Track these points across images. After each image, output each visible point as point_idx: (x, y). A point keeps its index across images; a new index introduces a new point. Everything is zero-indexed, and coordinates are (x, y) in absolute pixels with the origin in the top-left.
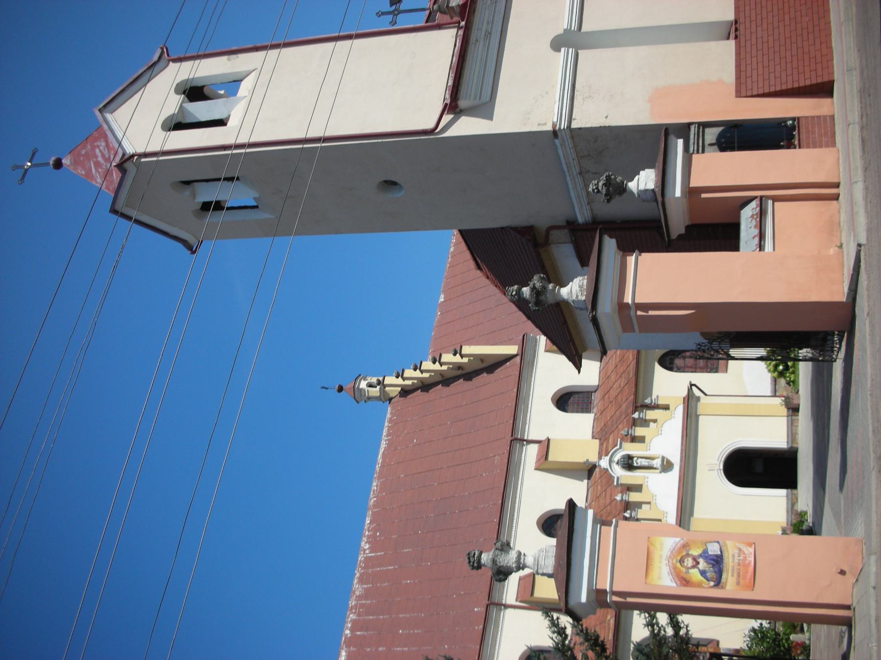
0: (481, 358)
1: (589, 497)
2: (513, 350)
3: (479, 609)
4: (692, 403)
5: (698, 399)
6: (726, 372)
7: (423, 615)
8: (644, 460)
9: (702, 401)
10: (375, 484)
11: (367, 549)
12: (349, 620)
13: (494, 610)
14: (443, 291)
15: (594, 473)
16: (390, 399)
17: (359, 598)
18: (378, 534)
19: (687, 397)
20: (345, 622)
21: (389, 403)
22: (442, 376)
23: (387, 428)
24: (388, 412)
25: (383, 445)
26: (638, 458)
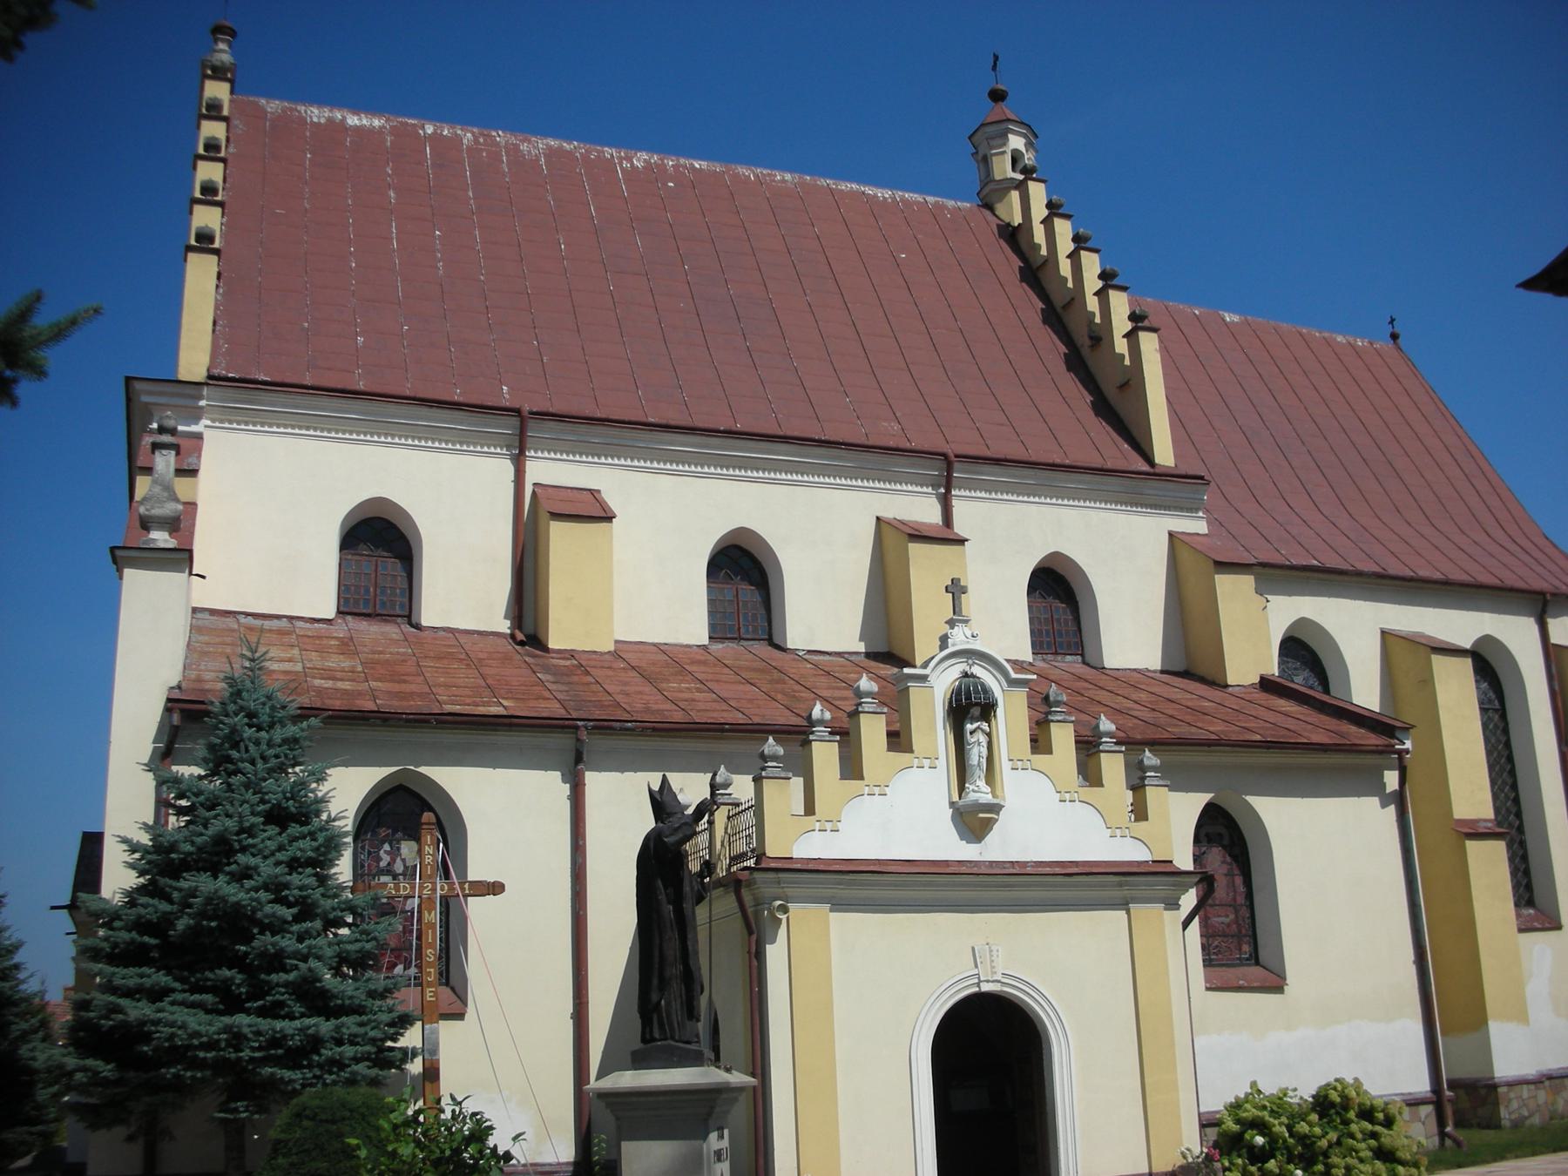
0: (1133, 381)
1: (821, 658)
2: (1164, 453)
3: (507, 396)
4: (1162, 887)
5: (1173, 905)
6: (1208, 989)
7: (482, 278)
8: (984, 752)
9: (1168, 915)
10: (788, 177)
11: (632, 164)
12: (459, 132)
13: (507, 427)
14: (1246, 320)
15: (888, 666)
16: (989, 206)
17: (514, 151)
18: (671, 184)
19: (1173, 870)
20: (452, 121)
21: (978, 205)
22: (1068, 305)
23: (921, 200)
24: (959, 204)
25: (884, 194)
26: (989, 735)
